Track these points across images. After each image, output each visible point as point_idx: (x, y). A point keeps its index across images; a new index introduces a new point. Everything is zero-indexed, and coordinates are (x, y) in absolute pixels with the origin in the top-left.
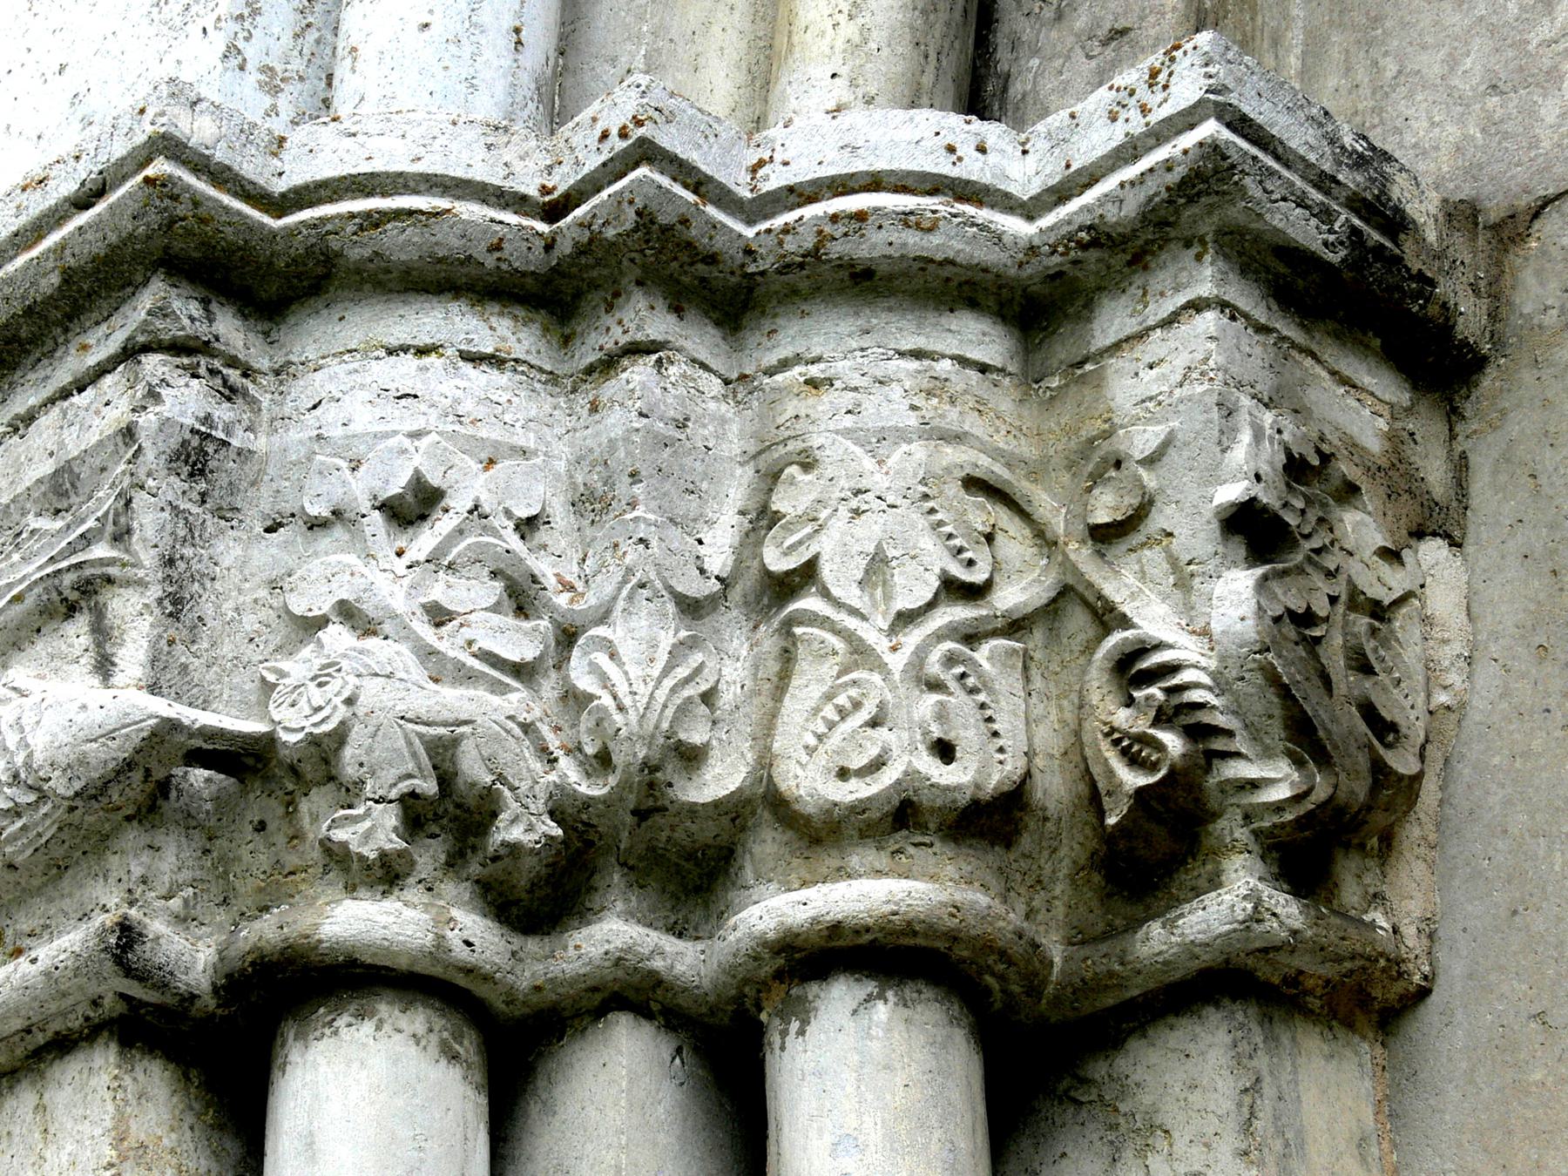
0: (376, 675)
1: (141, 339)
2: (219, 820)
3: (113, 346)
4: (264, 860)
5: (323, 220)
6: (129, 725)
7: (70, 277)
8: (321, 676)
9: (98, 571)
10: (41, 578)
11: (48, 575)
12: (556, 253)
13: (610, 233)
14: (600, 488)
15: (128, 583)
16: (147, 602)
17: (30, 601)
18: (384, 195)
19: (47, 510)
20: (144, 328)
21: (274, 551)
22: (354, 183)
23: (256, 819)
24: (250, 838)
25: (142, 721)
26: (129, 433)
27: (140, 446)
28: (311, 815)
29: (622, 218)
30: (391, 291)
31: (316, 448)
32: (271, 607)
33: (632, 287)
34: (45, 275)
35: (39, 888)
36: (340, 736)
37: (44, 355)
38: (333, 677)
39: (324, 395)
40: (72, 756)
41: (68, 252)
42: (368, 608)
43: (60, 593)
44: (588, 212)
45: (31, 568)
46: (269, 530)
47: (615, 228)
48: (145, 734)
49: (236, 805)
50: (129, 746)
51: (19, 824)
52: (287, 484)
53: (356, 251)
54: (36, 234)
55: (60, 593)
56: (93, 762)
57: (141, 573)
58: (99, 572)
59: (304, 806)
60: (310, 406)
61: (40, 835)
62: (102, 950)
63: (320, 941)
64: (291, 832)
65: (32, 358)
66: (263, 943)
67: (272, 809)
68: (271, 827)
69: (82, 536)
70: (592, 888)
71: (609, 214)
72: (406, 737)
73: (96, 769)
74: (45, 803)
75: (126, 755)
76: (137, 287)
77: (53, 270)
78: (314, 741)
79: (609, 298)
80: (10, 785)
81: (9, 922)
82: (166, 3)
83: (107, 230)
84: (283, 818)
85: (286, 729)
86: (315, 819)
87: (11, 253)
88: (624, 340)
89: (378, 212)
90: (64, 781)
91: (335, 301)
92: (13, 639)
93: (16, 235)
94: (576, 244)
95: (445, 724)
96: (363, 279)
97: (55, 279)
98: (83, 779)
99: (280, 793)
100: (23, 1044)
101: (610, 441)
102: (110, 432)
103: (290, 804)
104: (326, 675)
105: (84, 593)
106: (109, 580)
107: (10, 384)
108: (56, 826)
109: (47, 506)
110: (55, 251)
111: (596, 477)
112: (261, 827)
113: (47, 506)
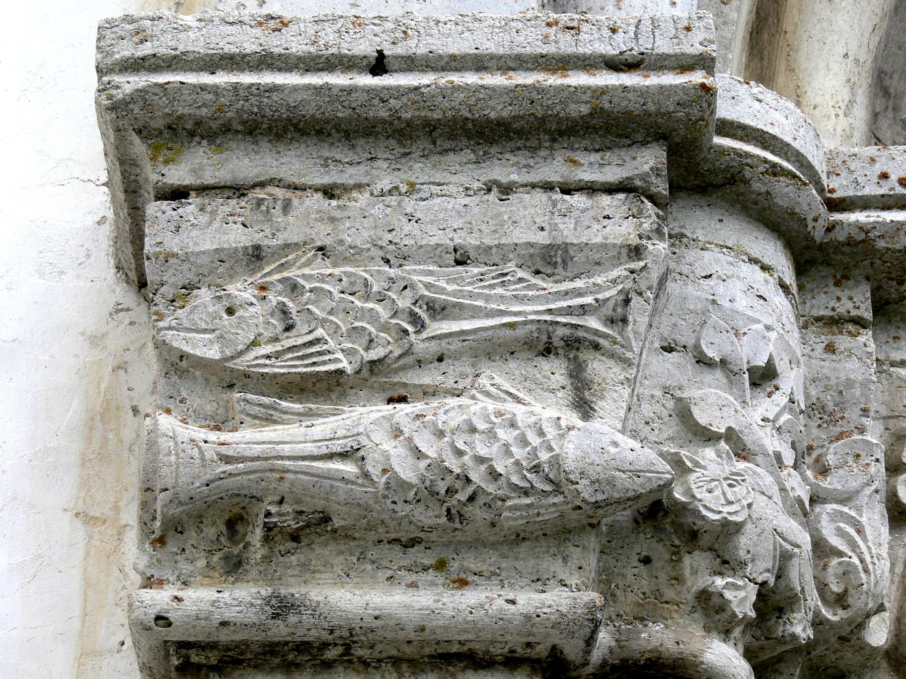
0: (763, 493)
1: (638, 183)
2: (609, 542)
3: (612, 175)
4: (645, 584)
5: (748, 155)
6: (653, 472)
7: (596, 113)
8: (730, 479)
9: (591, 337)
10: (539, 321)
11: (546, 321)
12: (832, 235)
13: (881, 244)
14: (830, 406)
15: (612, 356)
16: (628, 376)
17: (520, 332)
18: (772, 152)
19: (529, 267)
20: (644, 177)
21: (669, 366)
22: (761, 136)
23: (644, 554)
24: (635, 565)
25: (662, 473)
26: (636, 252)
27: (644, 267)
28: (692, 568)
29: (896, 239)
30: (751, 216)
31: (711, 308)
32: (663, 405)
33: (861, 278)
34: (578, 102)
35: (494, 544)
36: (738, 527)
37: (526, 147)
38: (739, 484)
39: (714, 272)
40: (602, 475)
41: (606, 98)
42: (748, 440)
43: (550, 337)
44: (870, 223)
45: (450, 288)
46: (664, 348)
47: (887, 243)
48: (662, 483)
49: (627, 537)
50: (648, 486)
51: (528, 501)
52: (683, 323)
53: (758, 185)
54: (561, 65)
55: (550, 337)
56: (619, 486)
57: (629, 355)
58: (591, 338)
59: (687, 560)
60: (704, 275)
61: (538, 514)
62: (588, 619)
63: (702, 663)
64: (673, 574)
65: (512, 144)
66: (663, 649)
67: (660, 553)
68: (656, 563)
69: (582, 306)
70: (777, 670)
71: (886, 232)
72: (775, 543)
73: (618, 492)
74: (556, 496)
75: (643, 491)
76: (634, 143)
77: (586, 103)
78: (725, 524)
79: (839, 277)
80: (529, 470)
81: (456, 557)
82: (820, 3)
83: (650, 100)
84: (667, 561)
85: (705, 507)
86: (694, 572)
87: (529, 65)
88: (854, 313)
89: (780, 167)
90: (591, 490)
91: (715, 205)
92: (490, 350)
93: (542, 57)
94: (850, 237)
95: (791, 544)
96: (738, 199)
97: (585, 109)
98: (606, 494)
99: (668, 543)
100: (436, 647)
101: (848, 379)
102: (619, 242)
103: (676, 557)
104: (734, 480)
105: (568, 345)
106: (596, 347)
107: (485, 153)
108: (558, 514)
109: (530, 264)
110: (595, 91)
111: (829, 398)
112: (646, 561)
113: (530, 264)
